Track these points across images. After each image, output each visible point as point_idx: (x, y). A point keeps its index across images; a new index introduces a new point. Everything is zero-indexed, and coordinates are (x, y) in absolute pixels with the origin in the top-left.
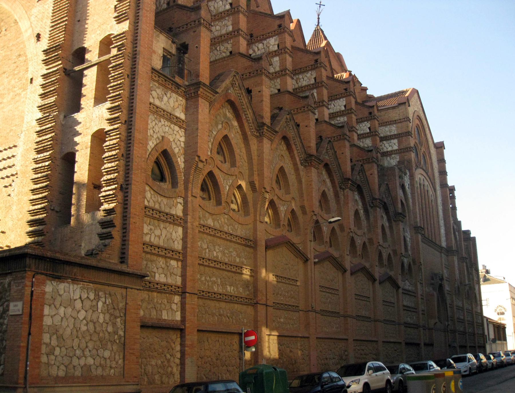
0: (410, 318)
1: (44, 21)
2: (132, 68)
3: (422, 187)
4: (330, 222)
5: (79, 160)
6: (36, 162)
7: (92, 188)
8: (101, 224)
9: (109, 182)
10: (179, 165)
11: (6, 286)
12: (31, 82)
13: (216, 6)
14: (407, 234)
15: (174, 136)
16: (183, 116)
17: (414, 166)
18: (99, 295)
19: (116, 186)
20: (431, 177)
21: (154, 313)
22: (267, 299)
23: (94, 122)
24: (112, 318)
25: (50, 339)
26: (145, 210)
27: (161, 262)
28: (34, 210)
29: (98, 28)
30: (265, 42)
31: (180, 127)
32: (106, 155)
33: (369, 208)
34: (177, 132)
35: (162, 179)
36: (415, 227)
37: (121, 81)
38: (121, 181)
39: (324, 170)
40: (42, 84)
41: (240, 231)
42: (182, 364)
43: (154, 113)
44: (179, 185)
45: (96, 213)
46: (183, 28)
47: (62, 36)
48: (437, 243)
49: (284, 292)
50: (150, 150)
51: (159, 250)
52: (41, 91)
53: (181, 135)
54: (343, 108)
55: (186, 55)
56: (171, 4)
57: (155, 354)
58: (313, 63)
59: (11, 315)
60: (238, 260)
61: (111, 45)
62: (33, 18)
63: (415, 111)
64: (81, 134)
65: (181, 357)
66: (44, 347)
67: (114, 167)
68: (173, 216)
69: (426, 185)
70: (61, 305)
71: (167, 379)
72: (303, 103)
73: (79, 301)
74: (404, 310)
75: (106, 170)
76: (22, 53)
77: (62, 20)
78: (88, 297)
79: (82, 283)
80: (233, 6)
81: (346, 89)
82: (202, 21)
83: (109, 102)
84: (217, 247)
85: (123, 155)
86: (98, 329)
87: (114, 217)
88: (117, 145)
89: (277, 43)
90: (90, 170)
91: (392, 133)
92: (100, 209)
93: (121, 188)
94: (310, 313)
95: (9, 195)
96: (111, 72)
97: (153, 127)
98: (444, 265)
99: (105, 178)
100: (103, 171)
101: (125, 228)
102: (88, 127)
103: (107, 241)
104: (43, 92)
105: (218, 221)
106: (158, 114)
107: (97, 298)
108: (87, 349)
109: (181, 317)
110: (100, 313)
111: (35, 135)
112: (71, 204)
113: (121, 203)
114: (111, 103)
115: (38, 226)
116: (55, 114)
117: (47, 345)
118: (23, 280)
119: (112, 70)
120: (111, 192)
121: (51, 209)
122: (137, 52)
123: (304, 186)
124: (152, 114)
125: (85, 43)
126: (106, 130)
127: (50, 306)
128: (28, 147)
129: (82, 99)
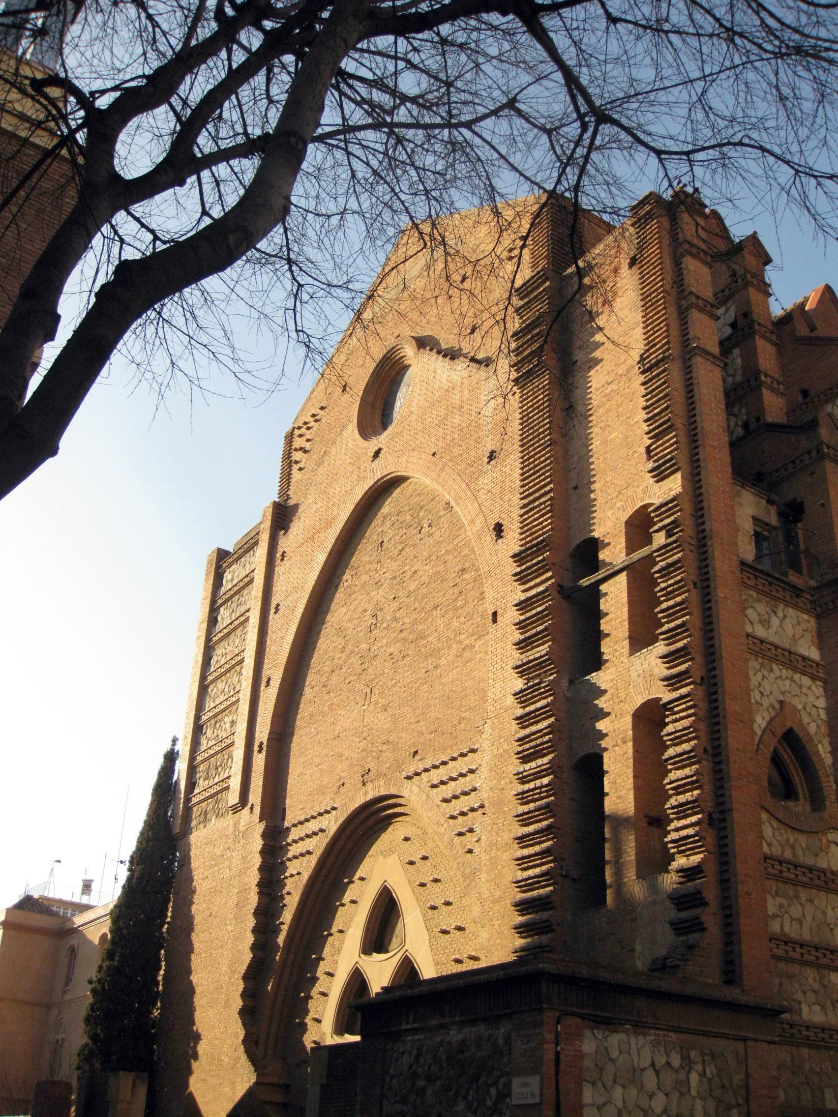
1: (506, 498)
2: (700, 568)
5: (612, 768)
6: (523, 779)
7: (645, 825)
8: (675, 901)
9: (683, 811)
10: (822, 759)
11: (501, 1042)
12: (495, 620)
15: (803, 698)
16: (814, 654)
18: (689, 1058)
19: (700, 816)
23: (635, 686)
26: (765, 864)
27: (810, 976)
28: (526, 880)
29: (617, 497)
31: (813, 678)
32: (671, 752)
34: (809, 688)
35: (788, 792)
37: (683, 596)
38: (709, 805)
40: (518, 621)
43: (756, 654)
44: (827, 803)
45: (660, 879)
46: (786, 470)
47: (547, 523)
50: (759, 733)
51: (804, 951)
52: (518, 636)
53: (818, 694)
55: (800, 525)
56: (753, 425)
59: (517, 1106)
61: (652, 527)
62: (482, 496)
64: (609, 714)
67: (691, 776)
68: (823, 871)
70: (615, 1082)
73: (650, 1071)
75: (675, 784)
76: (467, 565)
77: (542, 491)
78: (668, 1064)
79: (652, 1031)
82: (826, 450)
83: (662, 642)
85: (705, 751)
87: (702, 884)
88: (691, 730)
90: (637, 788)
92: (670, 868)
93: (709, 820)
95: (470, 851)
96: (659, 581)
97: (760, 685)
99: (673, 801)
100: (668, 787)
101: (729, 907)
102: (622, 698)
103: (692, 938)
104: (522, 637)
106: (765, 656)
107: (688, 1063)
110: (694, 1098)
111: (514, 725)
112: (602, 863)
113: (714, 854)
114: (667, 645)
115: (537, 912)
116: (552, 678)
118: (538, 1030)
119: (660, 577)
120: (691, 831)
121: (562, 876)
122: (707, 533)
124: (753, 657)
125: (594, 530)
126: (665, 700)
128: (501, 751)
129: (602, 643)
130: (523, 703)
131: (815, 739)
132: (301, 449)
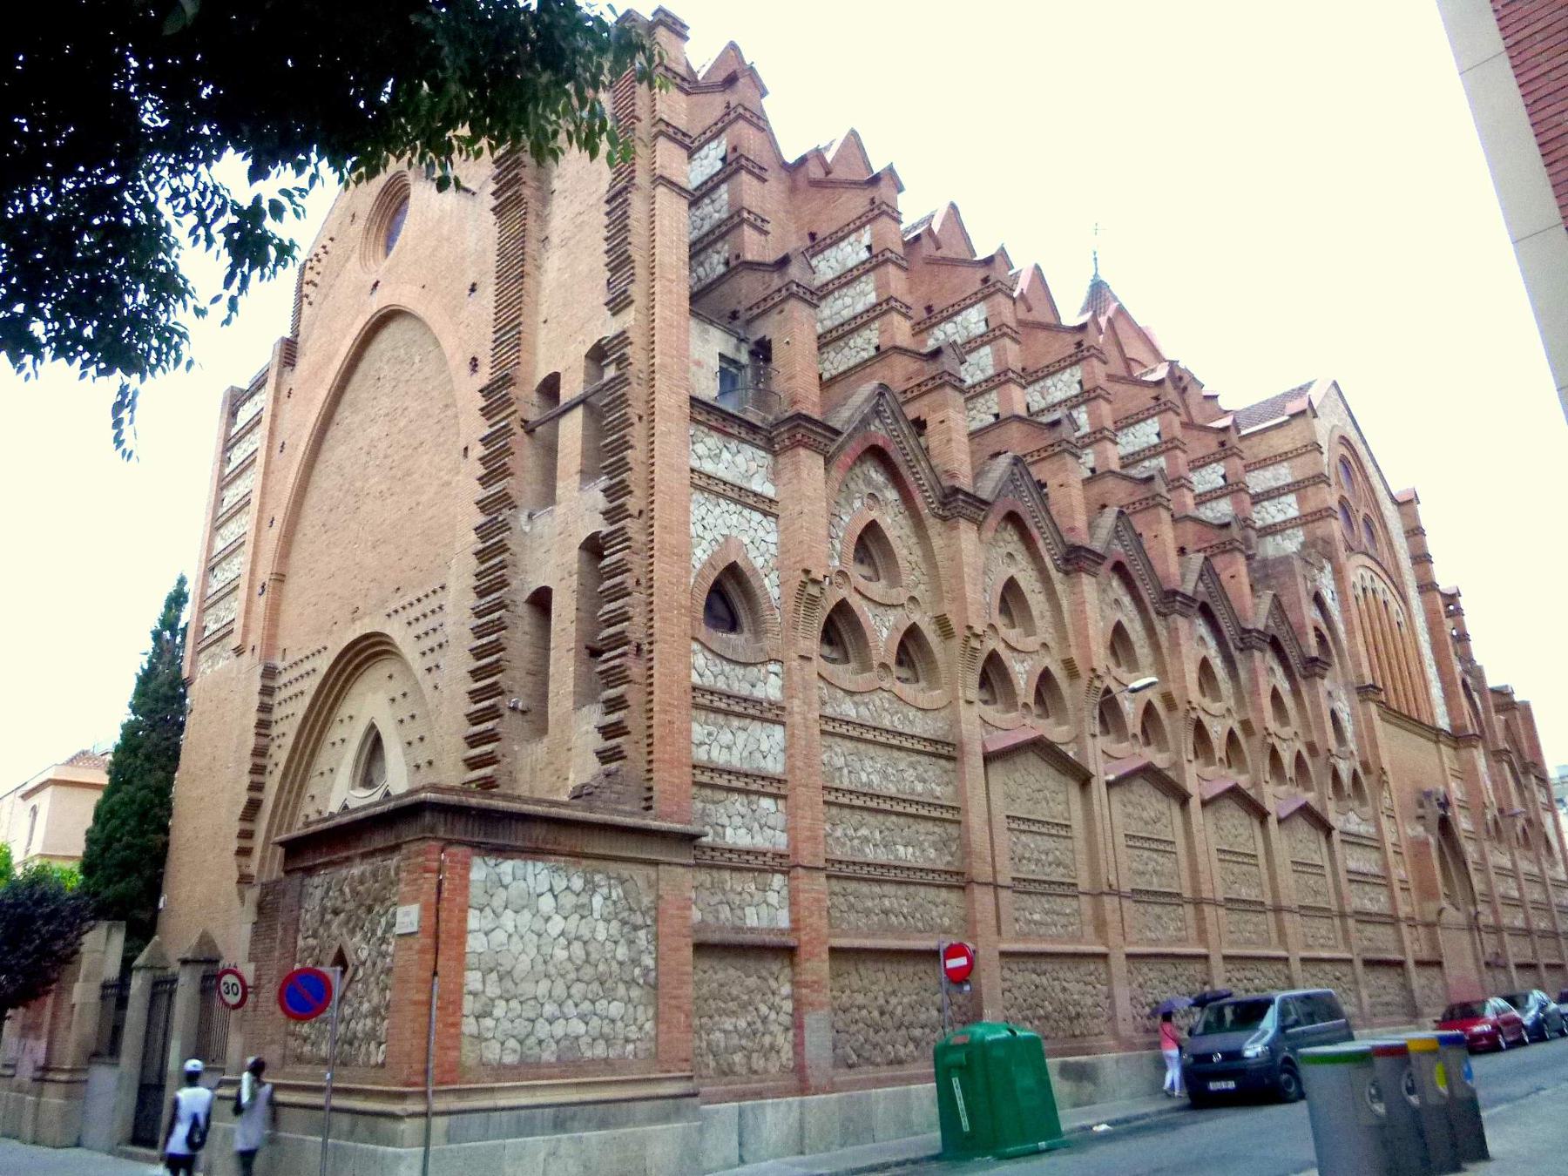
0: (1371, 900)
3: (1370, 594)
4: (1134, 691)
13: (840, 258)
14: (1341, 705)
15: (752, 532)
17: (1342, 548)
18: (593, 882)
20: (1392, 570)
21: (725, 912)
22: (995, 872)
24: (625, 930)
25: (484, 982)
27: (738, 803)
30: (958, 319)
33: (1236, 654)
36: (1358, 688)
39: (1116, 577)
41: (922, 726)
42: (798, 1025)
48: (1425, 719)
49: (1036, 853)
50: (698, 566)
52: (482, 471)
54: (1155, 440)
56: (733, 263)
57: (732, 1005)
58: (1072, 350)
59: (401, 935)
60: (919, 787)
63: (1334, 427)
65: (794, 1009)
66: (468, 1000)
69: (1380, 590)
71: (762, 1062)
72: (1050, 437)
73: (549, 895)
74: (1351, 881)
80: (875, 251)
81: (1157, 398)
84: (867, 763)
86: (594, 956)
89: (983, 317)
91: (1281, 483)
94: (1106, 899)
98: (1448, 772)
103: (613, 766)
105: (866, 704)
108: (570, 1002)
109: (792, 921)
111: (474, 561)
117: (475, 994)
123: (1066, 615)
126: (604, 533)
127: (481, 910)
130: (483, 538)
131: (762, 572)
132: (311, 282)
